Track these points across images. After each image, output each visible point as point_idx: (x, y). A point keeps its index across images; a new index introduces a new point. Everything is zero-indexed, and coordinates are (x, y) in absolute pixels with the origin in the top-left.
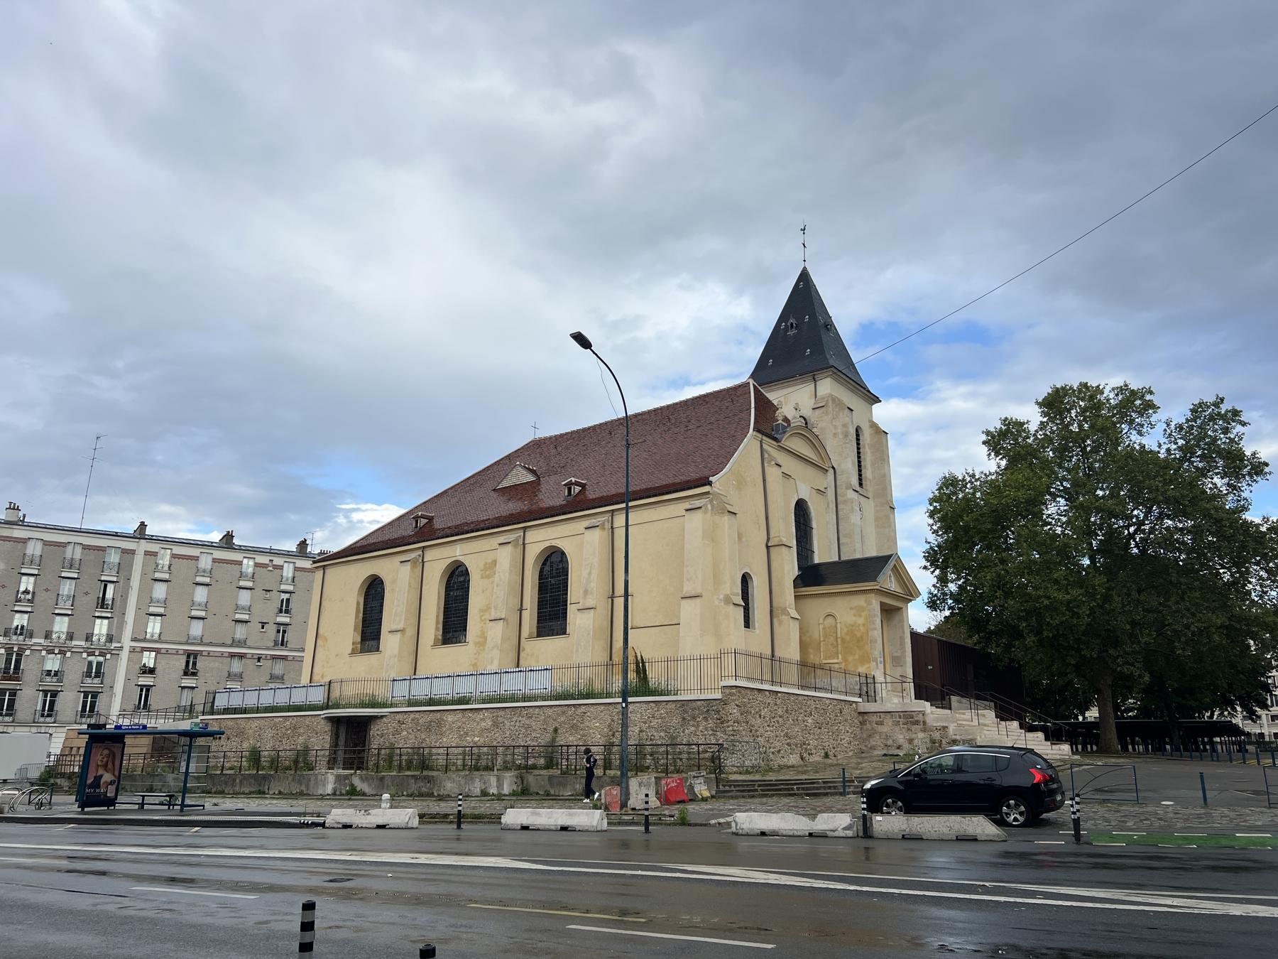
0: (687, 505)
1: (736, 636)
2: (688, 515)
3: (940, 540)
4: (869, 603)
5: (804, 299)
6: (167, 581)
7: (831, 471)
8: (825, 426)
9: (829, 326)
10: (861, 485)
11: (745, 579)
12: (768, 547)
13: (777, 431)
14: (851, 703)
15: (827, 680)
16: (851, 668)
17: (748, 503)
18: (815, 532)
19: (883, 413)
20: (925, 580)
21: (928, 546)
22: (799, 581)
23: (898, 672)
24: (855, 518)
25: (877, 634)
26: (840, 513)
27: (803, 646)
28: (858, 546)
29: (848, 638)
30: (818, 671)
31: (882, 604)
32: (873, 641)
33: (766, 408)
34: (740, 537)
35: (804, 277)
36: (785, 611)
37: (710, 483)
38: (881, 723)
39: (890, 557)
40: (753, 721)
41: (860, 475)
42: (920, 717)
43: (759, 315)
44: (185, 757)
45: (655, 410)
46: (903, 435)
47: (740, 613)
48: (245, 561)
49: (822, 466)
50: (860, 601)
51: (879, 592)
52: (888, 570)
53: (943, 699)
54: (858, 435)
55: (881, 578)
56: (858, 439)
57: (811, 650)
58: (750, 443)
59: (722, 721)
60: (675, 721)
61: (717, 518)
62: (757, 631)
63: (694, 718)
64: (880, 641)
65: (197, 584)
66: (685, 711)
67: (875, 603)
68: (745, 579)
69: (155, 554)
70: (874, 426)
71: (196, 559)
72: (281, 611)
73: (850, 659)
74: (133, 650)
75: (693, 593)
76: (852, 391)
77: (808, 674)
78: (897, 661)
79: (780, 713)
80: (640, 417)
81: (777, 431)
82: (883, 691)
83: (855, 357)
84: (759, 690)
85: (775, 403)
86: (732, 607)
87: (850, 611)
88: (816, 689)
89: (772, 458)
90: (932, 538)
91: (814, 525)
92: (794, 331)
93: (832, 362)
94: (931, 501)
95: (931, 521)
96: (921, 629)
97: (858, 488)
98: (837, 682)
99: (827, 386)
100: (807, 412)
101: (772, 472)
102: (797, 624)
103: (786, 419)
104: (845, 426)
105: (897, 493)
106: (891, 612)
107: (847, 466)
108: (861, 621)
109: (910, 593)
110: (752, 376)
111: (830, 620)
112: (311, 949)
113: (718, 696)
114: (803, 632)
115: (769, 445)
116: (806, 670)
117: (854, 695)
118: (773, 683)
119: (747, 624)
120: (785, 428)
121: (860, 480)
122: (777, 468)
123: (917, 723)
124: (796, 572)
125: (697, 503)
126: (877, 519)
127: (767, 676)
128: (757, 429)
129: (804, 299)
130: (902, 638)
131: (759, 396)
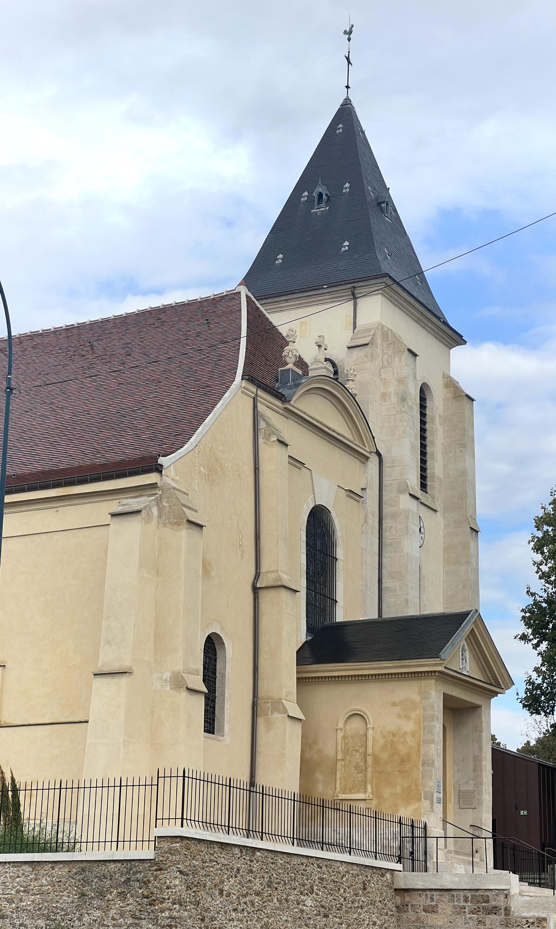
0: (115, 506)
1: (187, 747)
2: (116, 524)
3: (551, 589)
4: (425, 696)
5: (343, 152)
7: (374, 459)
8: (369, 379)
9: (384, 204)
10: (423, 487)
11: (212, 646)
12: (256, 590)
13: (285, 384)
14: (382, 871)
15: (343, 830)
16: (386, 809)
17: (226, 508)
18: (340, 567)
19: (467, 364)
20: (522, 661)
21: (530, 601)
22: (307, 653)
23: (467, 819)
24: (410, 546)
25: (435, 750)
26: (386, 534)
27: (307, 767)
28: (413, 594)
29: (384, 756)
30: (329, 814)
31: (447, 698)
32: (427, 763)
33: (267, 341)
34: (206, 568)
35: (346, 115)
36: (278, 705)
37: (159, 469)
38: (431, 910)
39: (466, 614)
40: (207, 901)
41: (423, 469)
42: (501, 902)
43: (263, 179)
44: (6, 834)
45: (69, 329)
46: (499, 406)
47: (200, 703)
49: (359, 448)
50: (409, 691)
51: (443, 677)
52: (460, 640)
53: (542, 869)
54: (423, 399)
55: (447, 652)
56: (423, 407)
57: (319, 776)
58: (236, 401)
59: (151, 900)
60: (67, 899)
61: (167, 532)
62: (227, 738)
63: (101, 894)
64: (439, 763)
66: (86, 882)
67: (434, 696)
68: (212, 646)
70: (452, 385)
73: (387, 792)
75: (115, 667)
76: (418, 321)
77: (313, 818)
78: (467, 800)
79: (257, 887)
80: (36, 339)
81: (285, 384)
82: (440, 852)
83: (426, 262)
84: (223, 845)
85: (283, 331)
86: (184, 694)
87: (394, 709)
88: (323, 845)
89: (272, 430)
90: (540, 587)
91: (340, 553)
92: (324, 208)
93: (386, 268)
94: (539, 523)
95: (539, 557)
96: (513, 744)
97: (418, 493)
98: (362, 835)
99: (375, 309)
100: (338, 352)
101: (271, 454)
102: (298, 728)
103: (301, 363)
104: (401, 381)
105: (484, 508)
106: (461, 713)
107: (402, 451)
108: (409, 726)
109: (494, 681)
110: (247, 281)
111: (356, 723)
113: (148, 853)
114: (307, 743)
115: (268, 407)
116: (309, 810)
117: (388, 857)
118: (248, 833)
119: (210, 725)
120: (297, 377)
121: (423, 477)
122: (278, 449)
123: (494, 910)
124: (302, 637)
125: (133, 503)
126: (447, 549)
127: (239, 820)
128: (248, 377)
129: (343, 152)
130: (477, 760)
131: (253, 310)
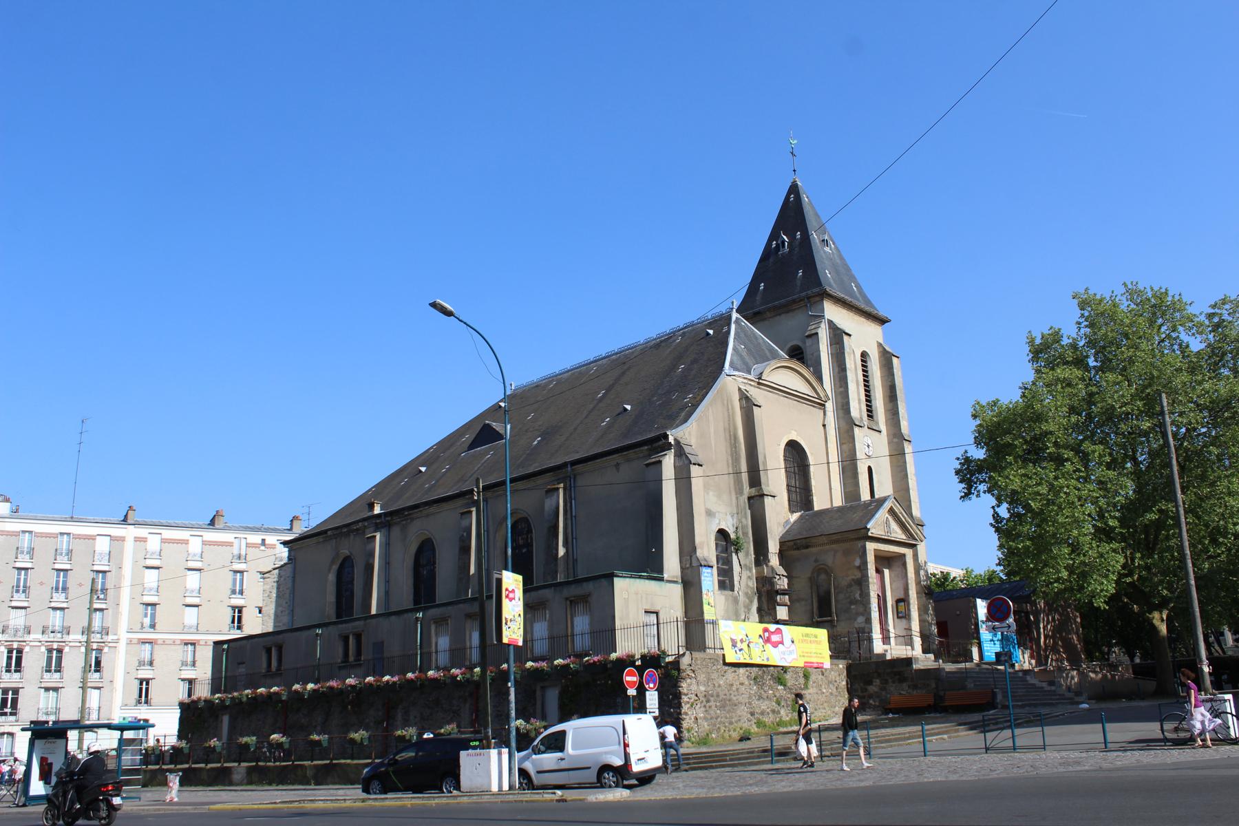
6: (199, 570)
35: (794, 189)
47: (259, 525)
48: (192, 540)
65: (147, 568)
69: (144, 540)
71: (186, 542)
72: (234, 592)
74: (130, 642)
112: (946, 623)
